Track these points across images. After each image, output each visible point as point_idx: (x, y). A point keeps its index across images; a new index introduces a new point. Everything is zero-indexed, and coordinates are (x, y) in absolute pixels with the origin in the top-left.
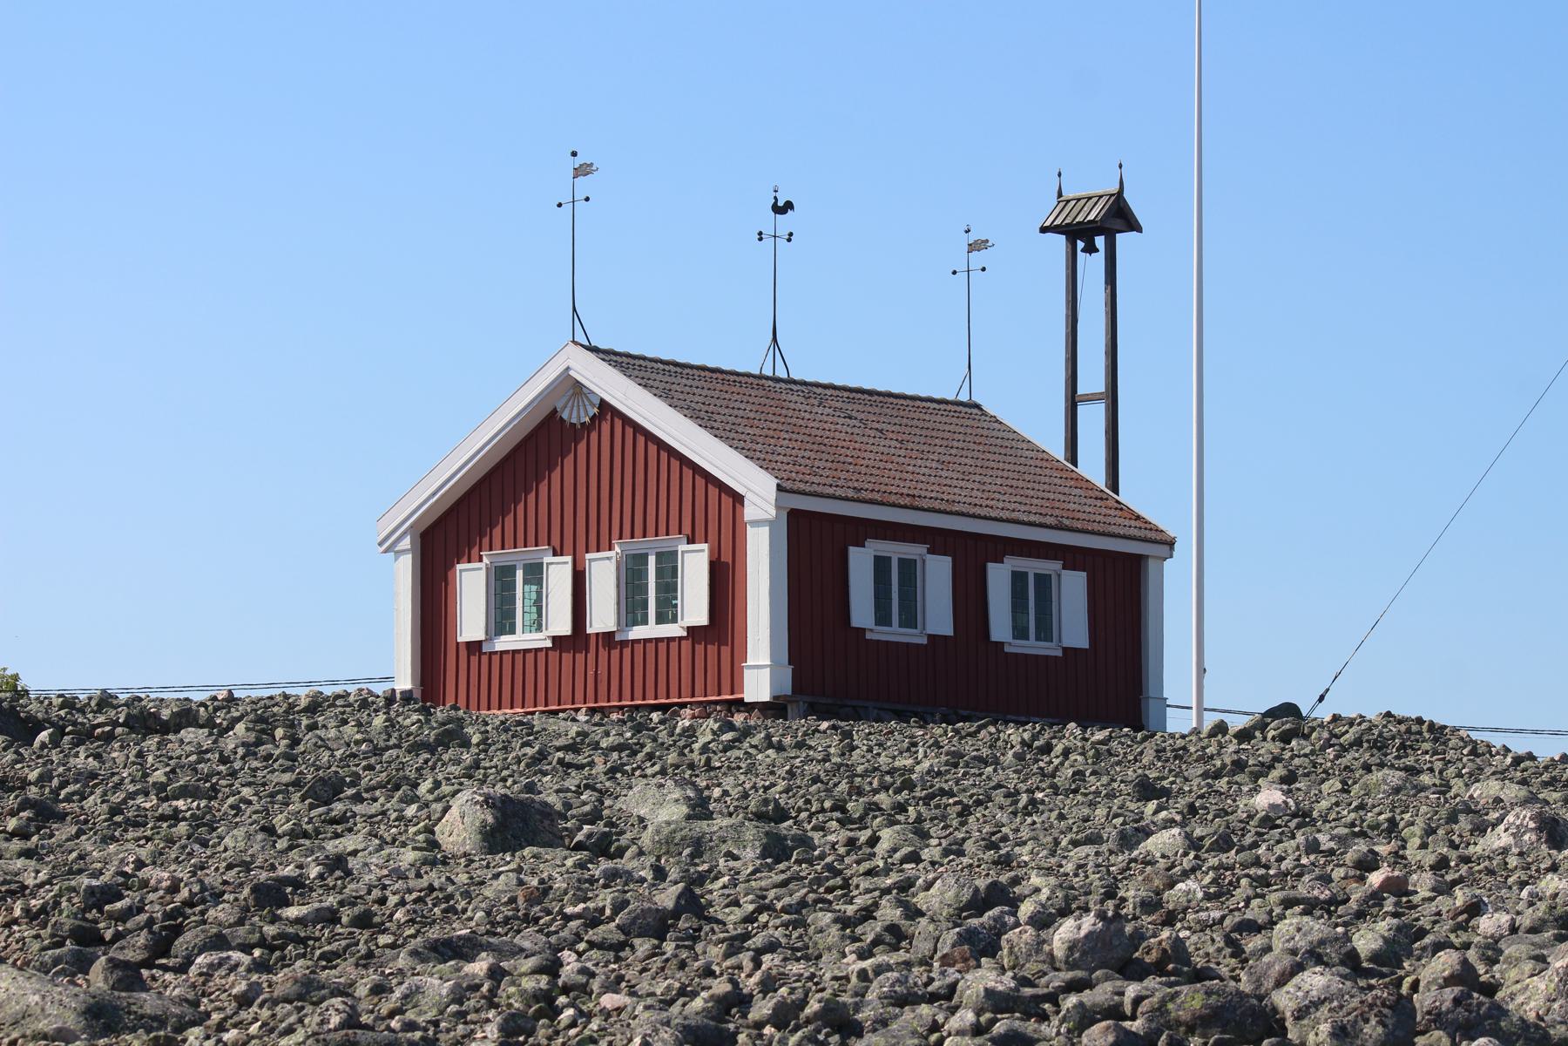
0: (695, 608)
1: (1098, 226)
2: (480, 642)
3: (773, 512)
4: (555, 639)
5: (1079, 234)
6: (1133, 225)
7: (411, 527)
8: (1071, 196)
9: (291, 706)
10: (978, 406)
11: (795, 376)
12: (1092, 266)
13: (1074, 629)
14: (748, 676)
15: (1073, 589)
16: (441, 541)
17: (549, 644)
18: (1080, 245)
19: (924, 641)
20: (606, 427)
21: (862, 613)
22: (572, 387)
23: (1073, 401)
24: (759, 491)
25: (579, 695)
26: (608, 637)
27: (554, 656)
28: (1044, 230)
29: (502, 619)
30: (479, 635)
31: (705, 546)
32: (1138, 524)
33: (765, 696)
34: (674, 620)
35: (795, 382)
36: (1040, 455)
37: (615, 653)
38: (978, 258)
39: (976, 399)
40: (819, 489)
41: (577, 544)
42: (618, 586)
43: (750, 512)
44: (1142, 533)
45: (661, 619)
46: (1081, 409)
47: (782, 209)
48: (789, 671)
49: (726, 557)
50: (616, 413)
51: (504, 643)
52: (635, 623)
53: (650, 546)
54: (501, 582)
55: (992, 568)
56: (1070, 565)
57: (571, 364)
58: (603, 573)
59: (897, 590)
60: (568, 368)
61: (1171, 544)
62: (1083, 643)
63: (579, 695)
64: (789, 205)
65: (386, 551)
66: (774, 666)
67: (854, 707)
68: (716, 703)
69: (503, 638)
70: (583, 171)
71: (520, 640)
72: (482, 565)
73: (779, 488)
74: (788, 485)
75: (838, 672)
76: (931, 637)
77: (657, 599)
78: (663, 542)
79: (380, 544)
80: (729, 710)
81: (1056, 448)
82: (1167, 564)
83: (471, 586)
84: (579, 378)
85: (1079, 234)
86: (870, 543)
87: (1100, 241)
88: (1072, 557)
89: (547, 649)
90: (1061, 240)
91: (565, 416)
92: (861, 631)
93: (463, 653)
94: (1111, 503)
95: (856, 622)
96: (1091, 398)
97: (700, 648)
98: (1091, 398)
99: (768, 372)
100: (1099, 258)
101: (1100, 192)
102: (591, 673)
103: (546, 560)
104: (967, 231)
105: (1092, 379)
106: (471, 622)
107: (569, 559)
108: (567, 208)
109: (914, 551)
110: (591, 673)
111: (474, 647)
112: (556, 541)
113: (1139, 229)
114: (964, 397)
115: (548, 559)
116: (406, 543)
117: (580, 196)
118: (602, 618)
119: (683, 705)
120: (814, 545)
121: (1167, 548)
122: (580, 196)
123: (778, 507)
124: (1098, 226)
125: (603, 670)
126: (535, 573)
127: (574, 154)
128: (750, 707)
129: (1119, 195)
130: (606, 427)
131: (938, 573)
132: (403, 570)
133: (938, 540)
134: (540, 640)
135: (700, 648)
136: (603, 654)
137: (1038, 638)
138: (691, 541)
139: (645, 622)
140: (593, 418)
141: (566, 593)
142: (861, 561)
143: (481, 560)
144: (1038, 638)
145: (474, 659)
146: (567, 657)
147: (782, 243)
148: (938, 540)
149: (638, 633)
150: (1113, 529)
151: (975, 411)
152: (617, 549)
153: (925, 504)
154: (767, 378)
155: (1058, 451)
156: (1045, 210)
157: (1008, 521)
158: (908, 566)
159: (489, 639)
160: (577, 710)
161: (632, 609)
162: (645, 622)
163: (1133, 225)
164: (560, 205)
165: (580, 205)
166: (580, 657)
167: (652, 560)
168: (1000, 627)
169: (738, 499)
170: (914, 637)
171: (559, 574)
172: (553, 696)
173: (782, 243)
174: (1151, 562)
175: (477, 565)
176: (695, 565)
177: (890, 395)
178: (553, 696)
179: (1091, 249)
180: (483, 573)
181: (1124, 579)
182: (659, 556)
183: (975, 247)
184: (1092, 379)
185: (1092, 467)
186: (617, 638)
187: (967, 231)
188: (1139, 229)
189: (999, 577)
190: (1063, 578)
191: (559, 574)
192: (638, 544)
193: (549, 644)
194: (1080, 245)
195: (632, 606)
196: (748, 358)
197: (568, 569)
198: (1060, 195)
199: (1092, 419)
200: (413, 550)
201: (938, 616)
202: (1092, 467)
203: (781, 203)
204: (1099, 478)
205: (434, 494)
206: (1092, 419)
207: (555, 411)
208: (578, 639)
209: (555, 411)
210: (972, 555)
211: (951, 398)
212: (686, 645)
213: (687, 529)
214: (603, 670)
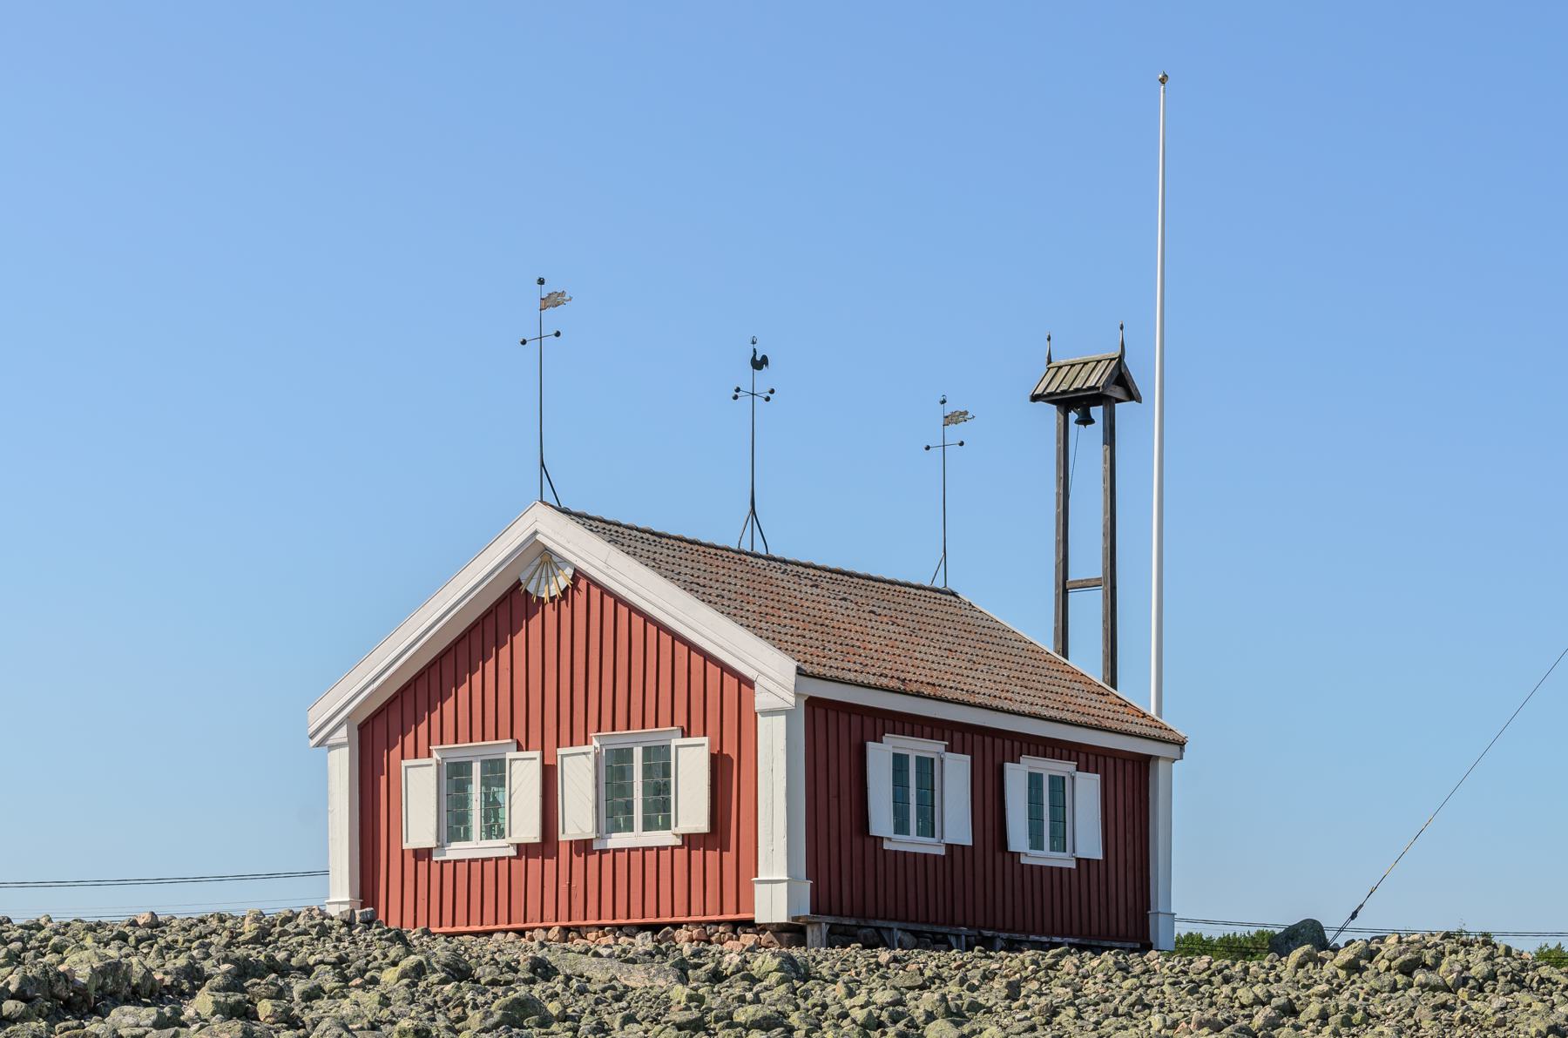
0: (692, 810)
1: (1091, 398)
3: (792, 700)
4: (519, 846)
5: (1075, 403)
6: (1132, 395)
7: (348, 717)
8: (1063, 362)
9: (234, 935)
10: (954, 594)
12: (1087, 440)
13: (1088, 841)
14: (761, 892)
15: (1087, 790)
16: (380, 732)
17: (513, 852)
18: (1073, 416)
19: (942, 851)
20: (580, 599)
21: (881, 821)
22: (542, 556)
23: (1064, 589)
24: (774, 677)
26: (583, 847)
27: (518, 865)
28: (1035, 398)
29: (454, 824)
30: (428, 841)
31: (705, 740)
32: (1144, 721)
33: (782, 917)
34: (666, 826)
35: (775, 560)
37: (593, 860)
38: (955, 432)
39: (951, 586)
40: (840, 674)
41: (549, 732)
42: (597, 786)
43: (762, 700)
44: (1146, 730)
45: (648, 825)
46: (1072, 596)
47: (759, 363)
48: (807, 886)
49: (730, 750)
50: (592, 582)
51: (457, 851)
52: (617, 829)
53: (475, 752)
55: (1009, 767)
57: (538, 526)
60: (536, 533)
61: (1181, 744)
64: (765, 360)
65: (319, 745)
66: (792, 881)
67: (877, 929)
68: (718, 923)
69: (454, 845)
70: (552, 301)
71: (476, 847)
72: (432, 761)
73: (800, 672)
74: (807, 668)
75: (859, 893)
76: (950, 847)
77: (644, 801)
79: (312, 737)
80: (734, 932)
81: (345, 728)
83: (418, 787)
84: (549, 544)
85: (1075, 403)
86: (887, 737)
87: (1097, 412)
89: (510, 858)
92: (878, 840)
93: (409, 861)
94: (1112, 699)
96: (1085, 585)
98: (1085, 585)
99: (746, 547)
102: (563, 886)
103: (510, 755)
104: (943, 402)
105: (1087, 562)
106: (418, 821)
107: (537, 754)
108: (533, 346)
110: (563, 886)
111: (422, 854)
112: (520, 733)
113: (1139, 400)
114: (939, 584)
115: (511, 754)
116: (342, 735)
117: (549, 330)
118: (578, 820)
119: (677, 926)
120: (837, 736)
122: (549, 330)
123: (797, 695)
124: (1091, 398)
126: (495, 772)
127: (541, 282)
128: (763, 928)
130: (580, 599)
131: (956, 772)
132: (340, 765)
133: (957, 735)
135: (697, 855)
137: (1052, 849)
138: (686, 733)
139: (629, 827)
141: (557, 787)
142: (880, 757)
143: (430, 755)
144: (1052, 849)
145: (422, 865)
146: (535, 864)
147: (759, 401)
148: (957, 735)
149: (617, 840)
150: (1108, 723)
151: (949, 598)
152: (596, 743)
153: (950, 694)
154: (747, 554)
155: (1046, 641)
157: (1030, 715)
158: (926, 765)
159: (441, 847)
160: (547, 929)
161: (614, 810)
163: (1132, 395)
164: (524, 342)
165: (550, 342)
167: (476, 767)
168: (1018, 838)
169: (745, 682)
171: (524, 774)
173: (759, 401)
174: (1161, 763)
175: (426, 761)
177: (869, 578)
179: (1086, 420)
180: (433, 771)
182: (647, 751)
184: (1087, 562)
185: (1087, 658)
187: (943, 402)
188: (1139, 400)
189: (1016, 776)
191: (524, 774)
193: (513, 852)
194: (1073, 416)
196: (727, 531)
197: (535, 769)
198: (1050, 362)
199: (1087, 608)
200: (350, 743)
201: (957, 827)
202: (1087, 658)
203: (758, 358)
204: (1097, 674)
205: (374, 680)
206: (1087, 608)
207: (519, 583)
208: (548, 843)
209: (519, 583)
210: (991, 749)
211: (927, 584)
212: (680, 855)
213: (681, 719)
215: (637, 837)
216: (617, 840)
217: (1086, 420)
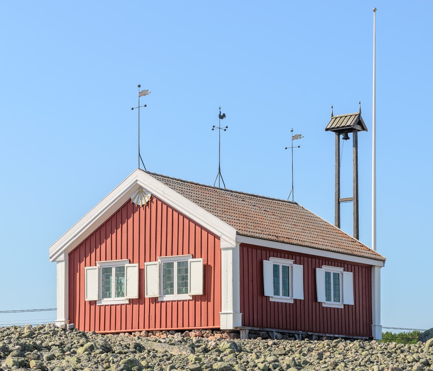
0: (196, 287)
1: (348, 130)
2: (95, 301)
7: (65, 250)
10: (296, 204)
11: (227, 188)
12: (347, 145)
13: (348, 298)
14: (223, 318)
15: (348, 278)
16: (77, 256)
20: (154, 206)
21: (269, 290)
25: (141, 325)
26: (154, 300)
28: (327, 130)
30: (95, 298)
31: (201, 259)
33: (230, 327)
36: (326, 224)
37: (158, 305)
38: (296, 142)
39: (295, 201)
40: (253, 234)
42: (160, 277)
43: (223, 244)
45: (179, 292)
46: (341, 204)
47: (222, 117)
49: (211, 263)
50: (158, 199)
51: (106, 301)
52: (168, 293)
53: (113, 264)
54: (106, 273)
56: (347, 270)
58: (153, 272)
59: (283, 279)
60: (137, 181)
61: (384, 261)
62: (351, 302)
63: (141, 325)
66: (235, 313)
67: (267, 332)
68: (206, 329)
69: (105, 299)
70: (143, 93)
71: (113, 300)
72: (97, 267)
73: (238, 234)
74: (240, 232)
76: (295, 300)
77: (178, 283)
78: (181, 258)
79: (51, 258)
81: (63, 255)
82: (382, 269)
83: (91, 276)
85: (342, 131)
87: (350, 135)
88: (347, 266)
90: (333, 135)
91: (135, 202)
92: (268, 297)
93: (88, 305)
95: (319, 300)
96: (346, 200)
97: (198, 303)
98: (346, 200)
100: (350, 141)
101: (346, 115)
103: (126, 265)
104: (292, 131)
105: (347, 192)
106: (91, 290)
107: (137, 265)
108: (136, 110)
109: (288, 262)
111: (93, 303)
115: (127, 265)
116: (62, 257)
119: (190, 330)
120: (251, 258)
121: (382, 262)
123: (237, 242)
124: (348, 130)
125: (152, 314)
126: (121, 271)
127: (139, 86)
128: (223, 331)
129: (359, 115)
131: (298, 272)
132: (61, 269)
133: (298, 257)
134: (123, 300)
135: (198, 303)
136: (152, 306)
137: (334, 301)
138: (194, 257)
139: (172, 293)
140: (148, 203)
141: (140, 278)
142: (268, 266)
143: (96, 265)
144: (334, 301)
146: (136, 306)
147: (222, 131)
148: (298, 257)
149: (168, 298)
151: (296, 205)
152: (159, 260)
154: (217, 188)
155: (332, 222)
156: (327, 122)
159: (100, 300)
160: (141, 332)
162: (172, 293)
164: (133, 109)
165: (142, 109)
166: (142, 306)
168: (321, 297)
170: (289, 300)
171: (132, 272)
172: (129, 325)
175: (94, 267)
176: (196, 269)
178: (129, 325)
179: (347, 138)
180: (97, 271)
181: (364, 275)
183: (295, 137)
184: (347, 192)
185: (347, 227)
186: (159, 300)
187: (292, 131)
189: (321, 273)
190: (344, 275)
191: (132, 272)
192: (169, 259)
193: (127, 302)
194: (342, 136)
195: (166, 285)
196: (210, 180)
198: (332, 116)
199: (347, 209)
201: (298, 292)
202: (347, 227)
203: (222, 115)
204: (351, 234)
206: (347, 209)
207: (130, 200)
209: (130, 200)
210: (310, 263)
211: (286, 200)
212: (192, 303)
213: (192, 252)
214: (152, 314)
215: (175, 297)
216: (168, 298)
217: (347, 138)
